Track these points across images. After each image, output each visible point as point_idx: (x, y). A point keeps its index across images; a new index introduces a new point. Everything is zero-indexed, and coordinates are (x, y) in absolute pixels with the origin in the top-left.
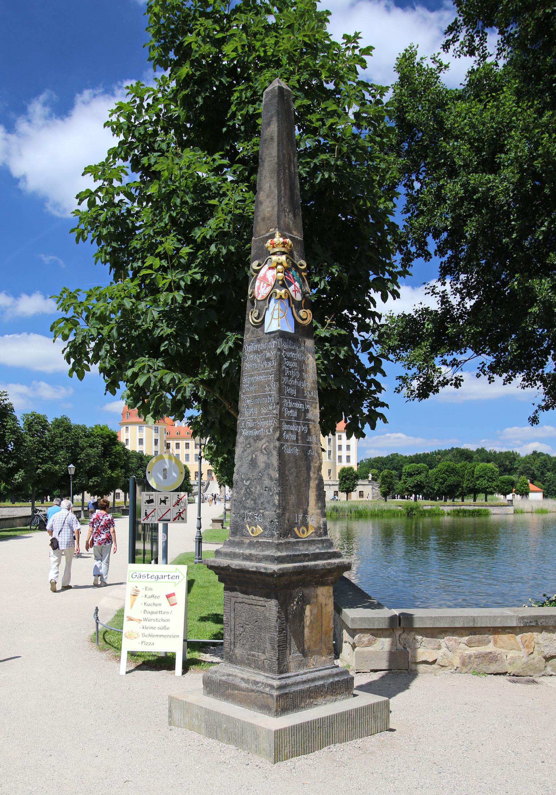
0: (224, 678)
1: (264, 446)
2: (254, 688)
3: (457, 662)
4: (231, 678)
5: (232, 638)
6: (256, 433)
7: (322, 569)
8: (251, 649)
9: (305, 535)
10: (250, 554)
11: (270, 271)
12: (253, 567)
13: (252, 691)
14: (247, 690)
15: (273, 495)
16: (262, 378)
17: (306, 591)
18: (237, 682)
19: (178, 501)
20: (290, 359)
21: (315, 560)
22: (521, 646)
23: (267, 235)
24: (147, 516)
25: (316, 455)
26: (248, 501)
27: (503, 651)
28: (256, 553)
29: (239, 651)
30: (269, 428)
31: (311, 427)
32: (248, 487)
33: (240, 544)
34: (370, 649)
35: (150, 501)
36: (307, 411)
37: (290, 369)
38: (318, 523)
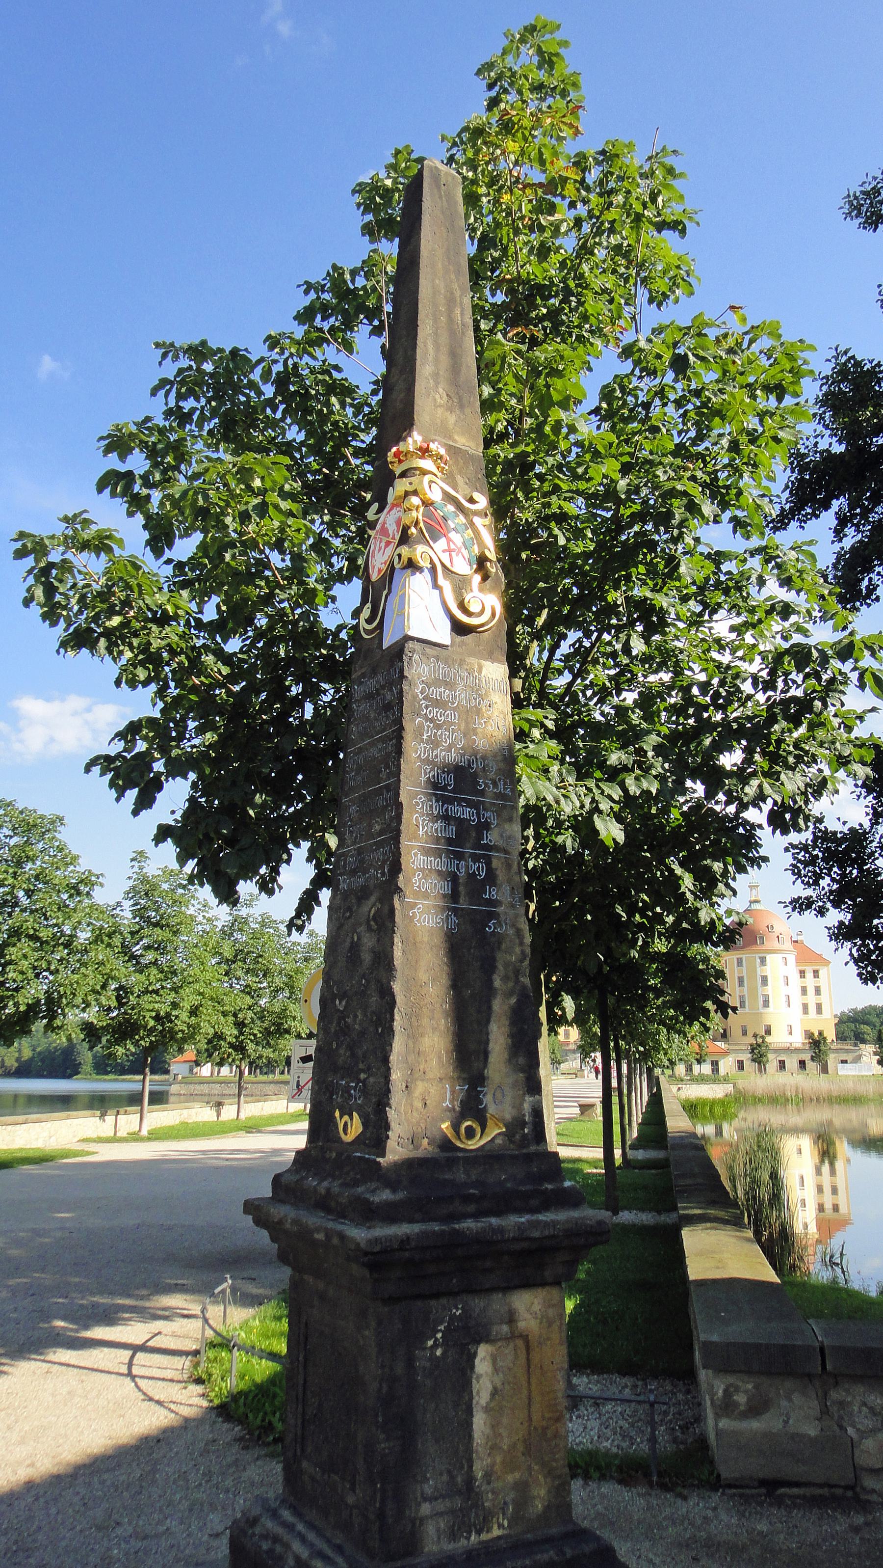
7: (515, 1239)
9: (473, 1144)
17: (477, 1303)
20: (438, 703)
21: (498, 1214)
25: (511, 932)
31: (495, 863)
34: (755, 1425)
36: (485, 826)
37: (438, 727)
38: (519, 1107)
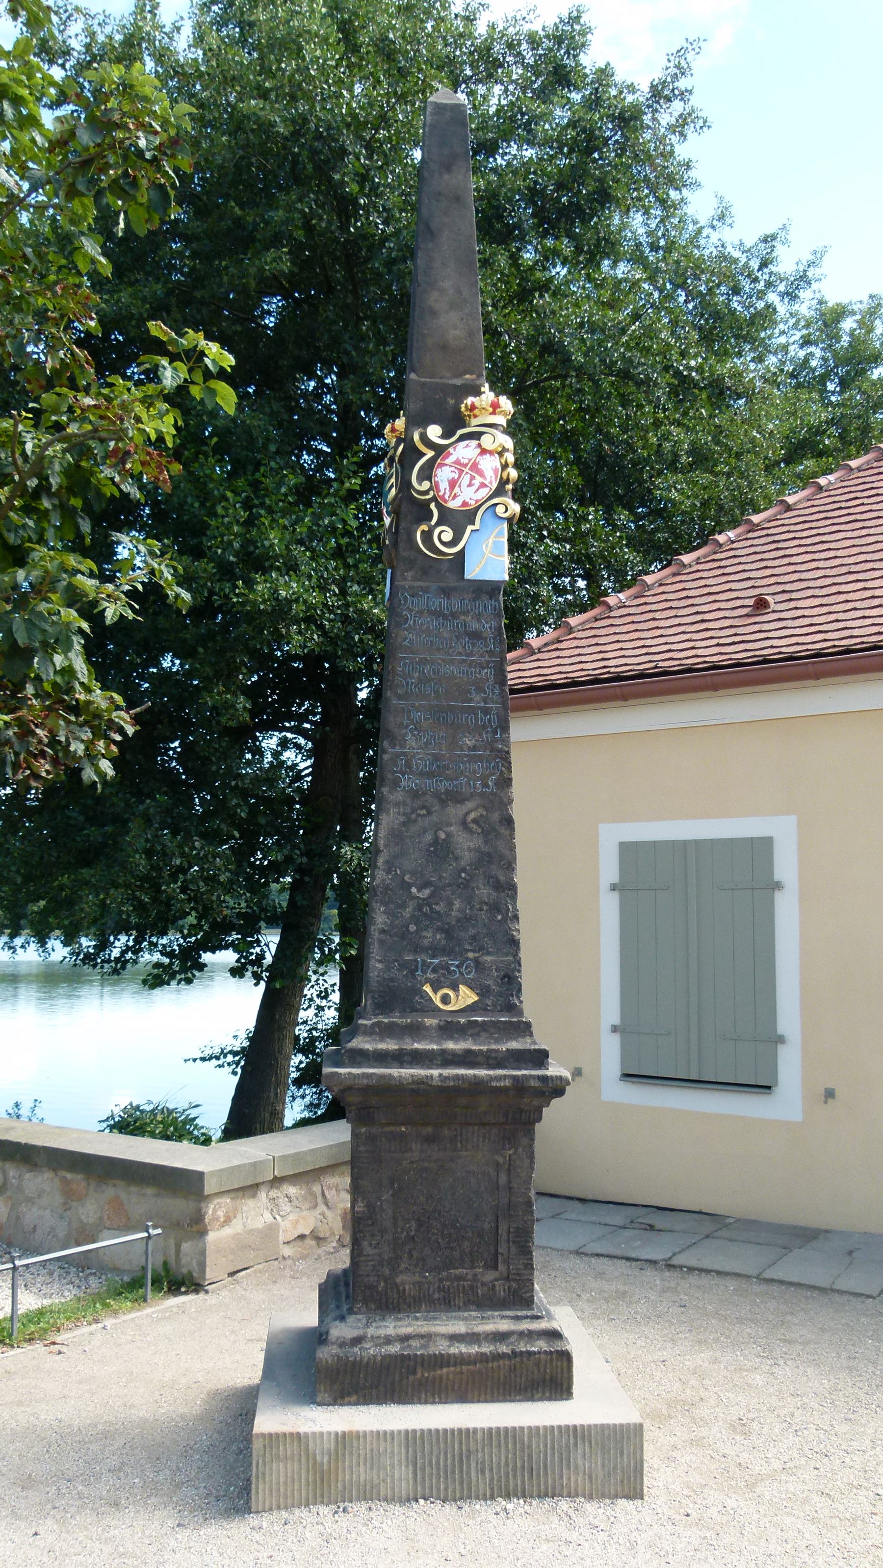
0: (395, 1349)
1: (473, 815)
2: (504, 1349)
4: (414, 1343)
8: (449, 1264)
10: (468, 1052)
14: (483, 1358)
18: (442, 1347)
23: (458, 382)
26: (428, 934)
28: (484, 1048)
29: (406, 1279)
32: (426, 902)
33: (416, 1031)
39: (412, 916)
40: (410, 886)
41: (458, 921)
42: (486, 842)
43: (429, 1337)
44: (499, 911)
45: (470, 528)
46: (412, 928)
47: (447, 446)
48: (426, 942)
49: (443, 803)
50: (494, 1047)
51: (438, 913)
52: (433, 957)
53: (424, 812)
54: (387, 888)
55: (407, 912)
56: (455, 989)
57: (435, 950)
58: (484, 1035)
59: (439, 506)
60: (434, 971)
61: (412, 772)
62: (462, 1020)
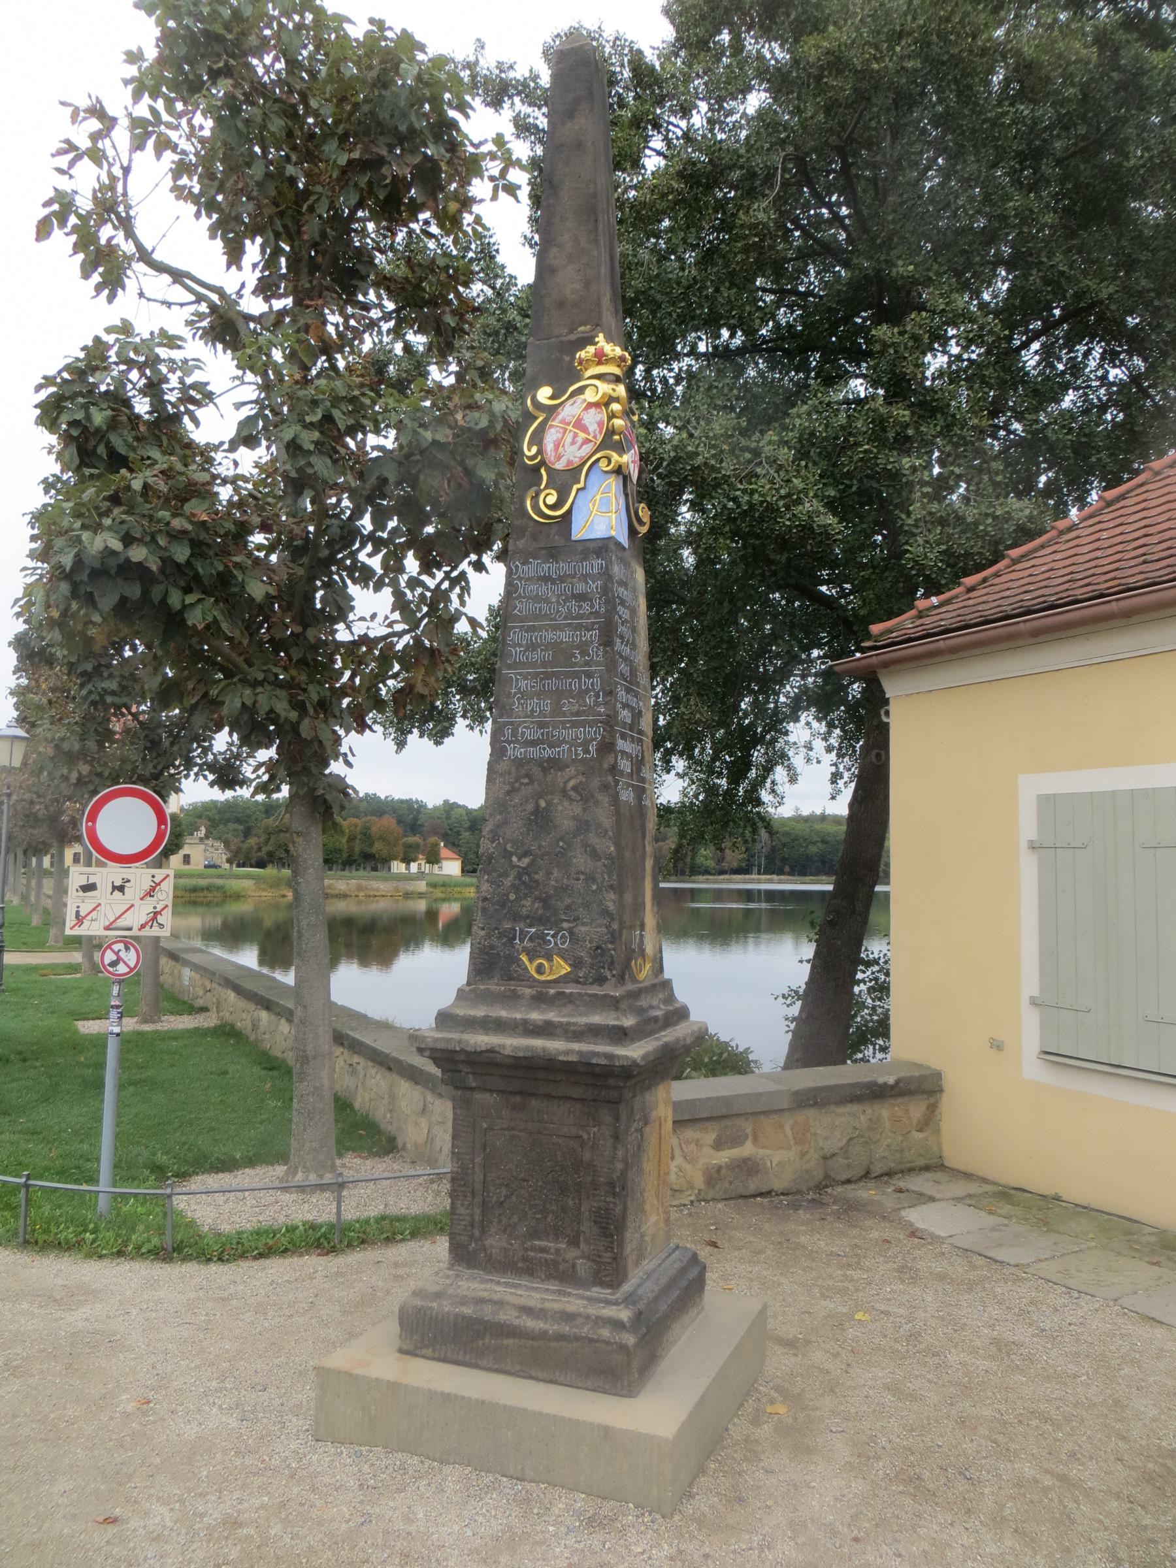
0: (467, 1311)
1: (572, 783)
2: (566, 1329)
3: (699, 1181)
5: (478, 1211)
6: (548, 752)
8: (534, 1234)
11: (592, 411)
12: (567, 1053)
13: (560, 1337)
14: (543, 1335)
15: (599, 889)
16: (565, 636)
18: (507, 1316)
19: (153, 889)
22: (792, 1142)
23: (572, 337)
24: (80, 919)
26: (527, 903)
27: (768, 1152)
30: (585, 745)
32: (525, 871)
33: (512, 998)
35: (89, 888)
39: (513, 885)
40: (511, 854)
41: (555, 889)
42: (584, 810)
43: (501, 1303)
44: (594, 880)
45: (575, 487)
46: (512, 897)
47: (556, 407)
48: (524, 911)
49: (545, 770)
50: (573, 1020)
51: (537, 882)
52: (531, 926)
53: (526, 781)
54: (490, 858)
55: (508, 881)
56: (549, 959)
57: (533, 920)
58: (570, 1007)
59: (548, 470)
60: (531, 939)
61: (517, 742)
62: (552, 991)
